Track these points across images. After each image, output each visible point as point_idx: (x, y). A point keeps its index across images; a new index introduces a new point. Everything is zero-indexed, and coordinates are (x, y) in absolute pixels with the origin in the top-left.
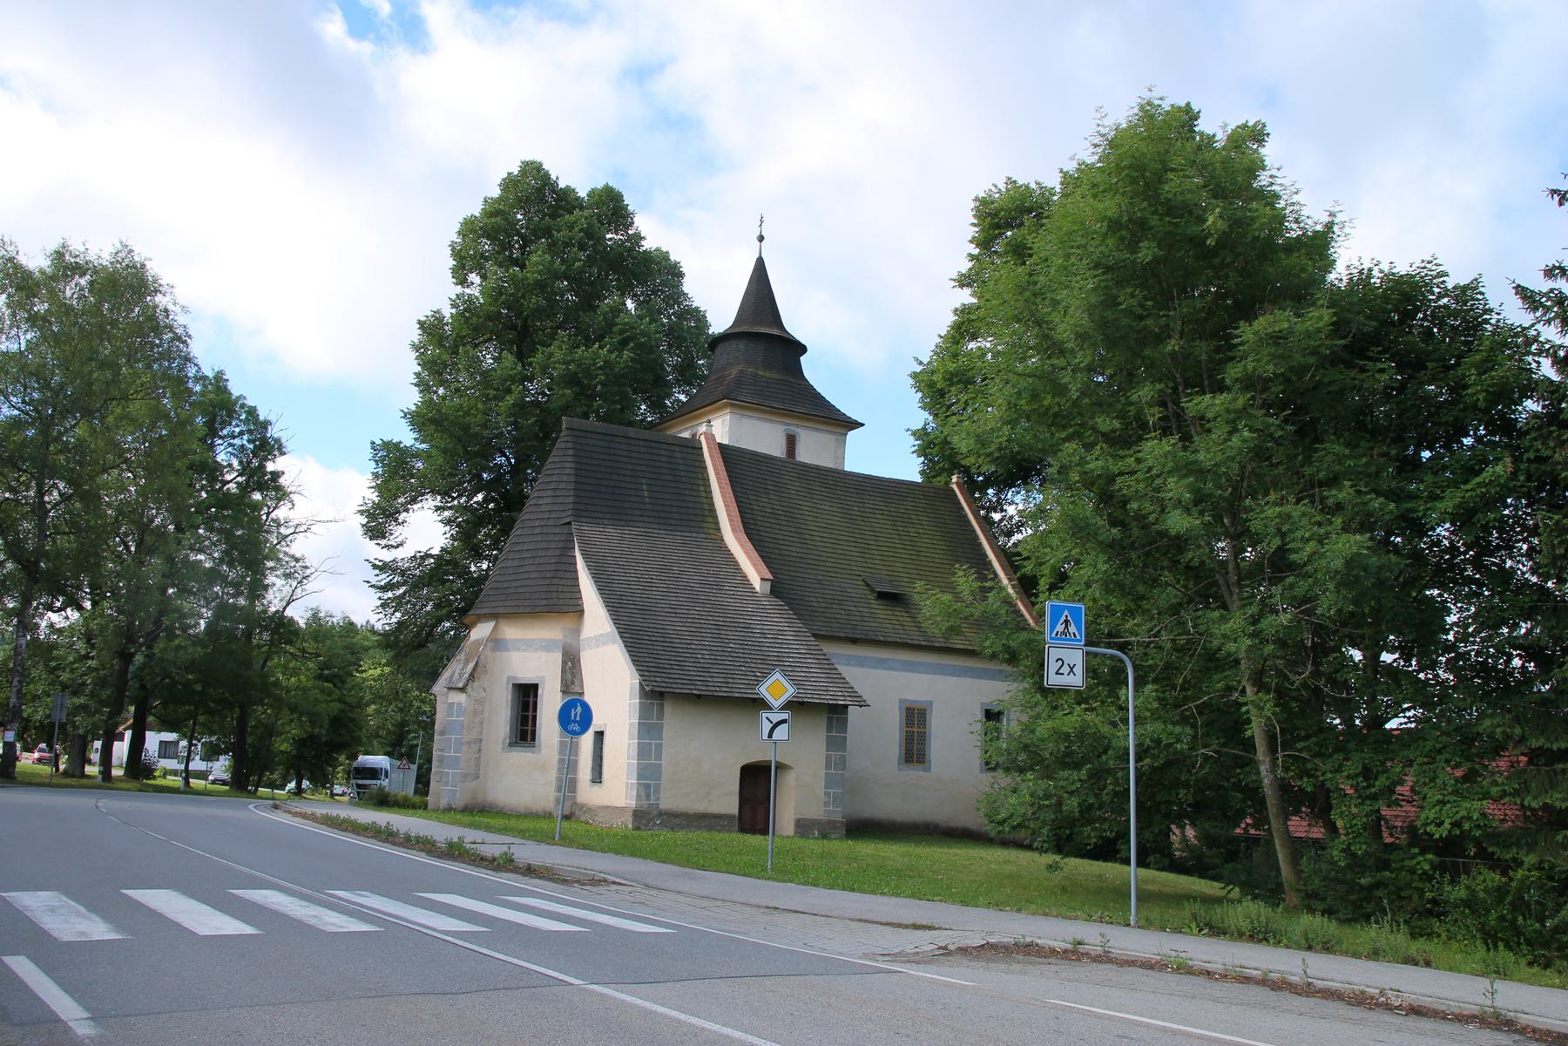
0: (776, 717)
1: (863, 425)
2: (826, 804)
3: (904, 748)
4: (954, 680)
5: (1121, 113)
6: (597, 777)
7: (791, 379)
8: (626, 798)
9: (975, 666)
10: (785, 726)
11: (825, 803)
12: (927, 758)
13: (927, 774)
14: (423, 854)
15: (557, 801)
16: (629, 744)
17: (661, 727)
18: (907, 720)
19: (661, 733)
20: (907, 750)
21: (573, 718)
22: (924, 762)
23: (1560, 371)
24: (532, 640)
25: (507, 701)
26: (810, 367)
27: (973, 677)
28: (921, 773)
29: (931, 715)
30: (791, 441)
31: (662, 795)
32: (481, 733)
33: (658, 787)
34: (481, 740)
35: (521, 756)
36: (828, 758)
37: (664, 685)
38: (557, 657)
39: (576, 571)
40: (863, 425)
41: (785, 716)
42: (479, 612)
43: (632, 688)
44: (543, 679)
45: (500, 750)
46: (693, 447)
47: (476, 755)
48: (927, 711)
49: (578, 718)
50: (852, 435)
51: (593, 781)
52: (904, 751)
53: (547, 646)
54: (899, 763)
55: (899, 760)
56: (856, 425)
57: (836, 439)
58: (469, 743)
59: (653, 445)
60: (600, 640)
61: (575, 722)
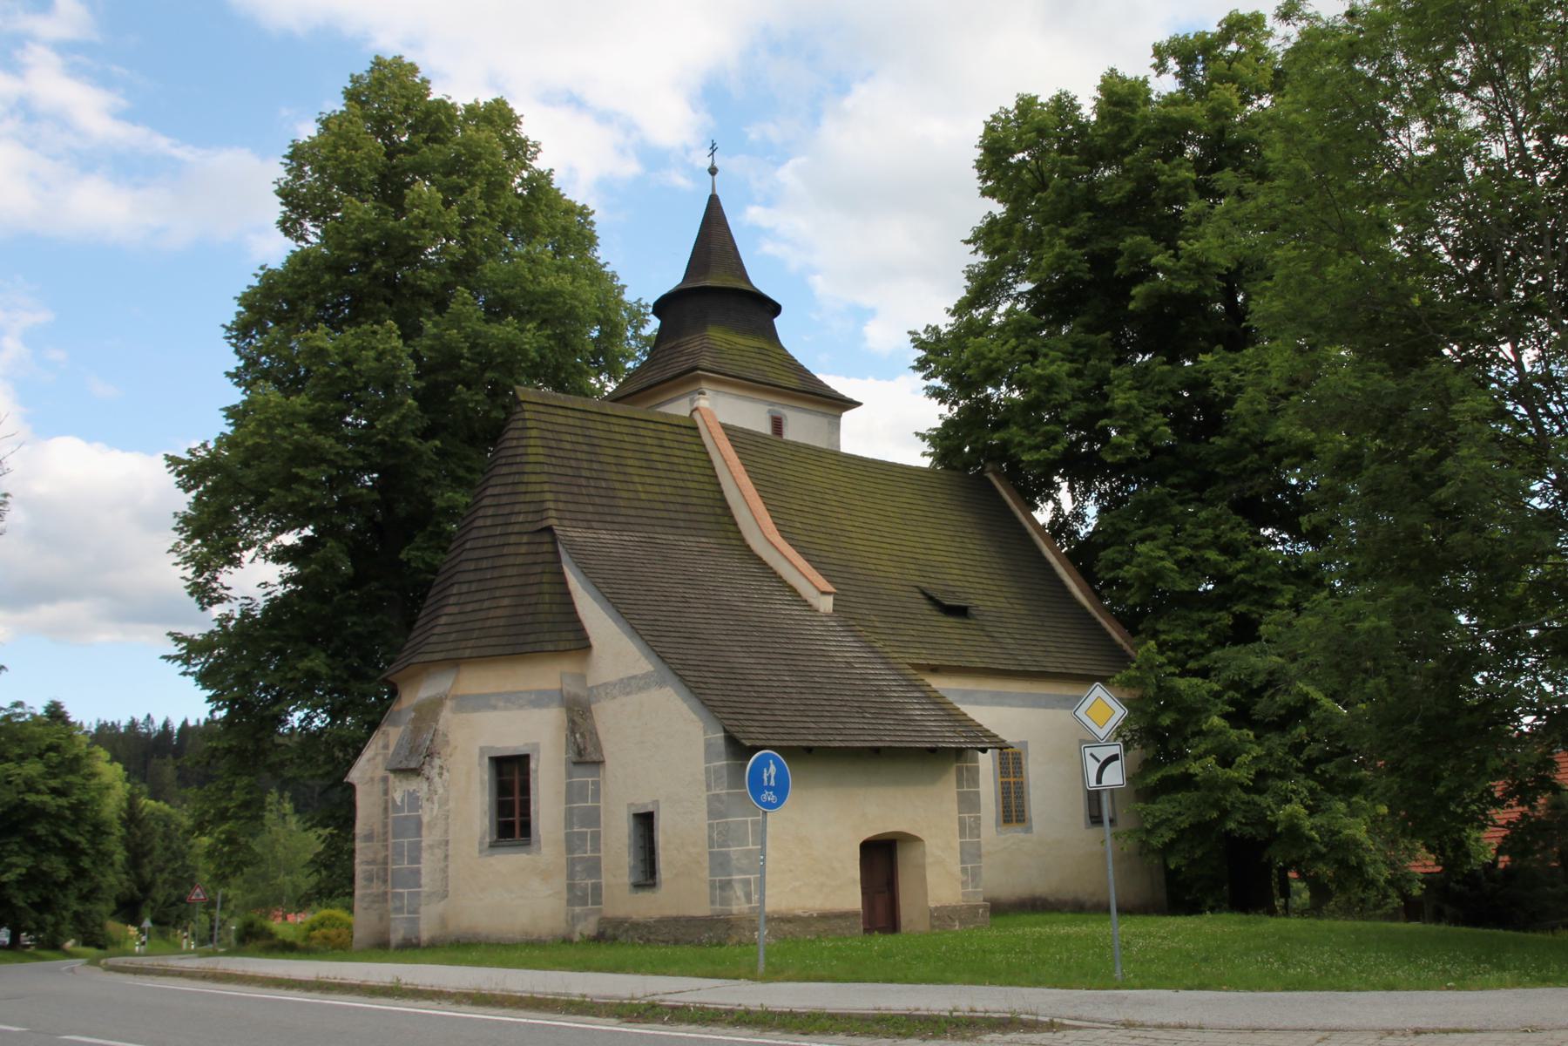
0: (1104, 753)
1: (859, 404)
2: (964, 884)
4: (1050, 712)
5: (1225, 14)
8: (713, 902)
9: (1058, 692)
10: (1116, 765)
14: (613, 1021)
18: (1002, 768)
20: (1004, 807)
21: (766, 783)
23: (1101, 427)
25: (482, 782)
28: (1022, 835)
30: (777, 424)
32: (446, 831)
35: (510, 861)
36: (962, 823)
40: (859, 404)
41: (1115, 750)
42: (427, 658)
44: (536, 746)
45: (476, 854)
46: (691, 428)
47: (442, 865)
49: (773, 783)
50: (847, 417)
51: (638, 886)
52: (1001, 809)
53: (539, 700)
54: (997, 826)
55: (997, 821)
56: (851, 404)
57: (829, 423)
58: (431, 847)
60: (628, 685)
61: (769, 788)
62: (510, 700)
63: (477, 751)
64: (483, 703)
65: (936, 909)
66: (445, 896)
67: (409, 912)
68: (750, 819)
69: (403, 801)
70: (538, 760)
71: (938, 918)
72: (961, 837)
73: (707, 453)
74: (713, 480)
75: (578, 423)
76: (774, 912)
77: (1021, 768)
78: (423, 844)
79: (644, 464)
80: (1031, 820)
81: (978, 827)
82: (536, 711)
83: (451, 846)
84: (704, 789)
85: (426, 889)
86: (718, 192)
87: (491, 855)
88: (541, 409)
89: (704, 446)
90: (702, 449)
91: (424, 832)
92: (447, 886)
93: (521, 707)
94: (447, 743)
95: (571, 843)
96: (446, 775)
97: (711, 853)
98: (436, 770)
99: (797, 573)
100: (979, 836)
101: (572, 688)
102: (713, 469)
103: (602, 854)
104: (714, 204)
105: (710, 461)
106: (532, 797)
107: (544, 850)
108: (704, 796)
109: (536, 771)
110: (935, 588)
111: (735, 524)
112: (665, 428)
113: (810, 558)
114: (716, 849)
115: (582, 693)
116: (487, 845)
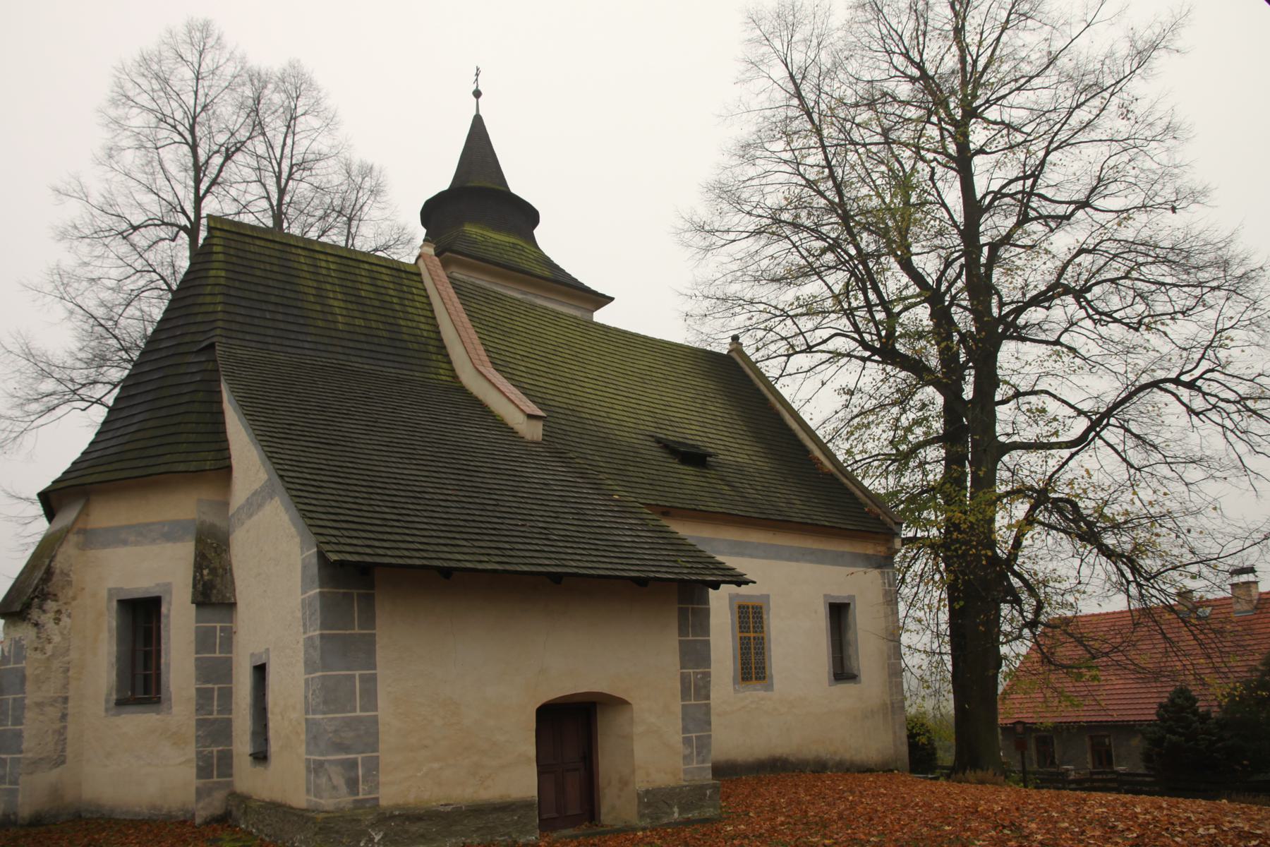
1: (612, 299)
2: (686, 758)
3: (739, 661)
6: (261, 757)
7: (525, 245)
8: (308, 791)
11: (685, 757)
12: (767, 673)
13: (769, 693)
15: (200, 793)
16: (307, 681)
17: (370, 643)
19: (371, 652)
22: (764, 678)
24: (148, 525)
26: (546, 238)
27: (811, 562)
28: (762, 693)
29: (768, 613)
31: (382, 778)
32: (65, 686)
33: (373, 766)
34: (66, 700)
35: (138, 721)
36: (684, 680)
37: (368, 551)
38: (186, 551)
39: (222, 413)
40: (612, 299)
43: (305, 567)
45: (103, 714)
47: (58, 726)
48: (764, 610)
52: (739, 666)
53: (171, 533)
55: (120, 590)
58: (40, 705)
59: (351, 263)
62: (142, 533)
63: (105, 594)
64: (116, 537)
65: (647, 792)
66: (60, 761)
67: (11, 783)
68: (357, 673)
69: (9, 652)
70: (170, 603)
71: (648, 805)
72: (683, 699)
73: (428, 297)
74: (430, 321)
75: (278, 254)
76: (397, 807)
77: (761, 622)
78: (27, 701)
79: (353, 299)
80: (771, 677)
81: (707, 686)
82: (169, 545)
83: (70, 704)
84: (302, 630)
85: (30, 755)
86: (481, 113)
87: (118, 714)
88: (235, 237)
89: (425, 290)
90: (423, 293)
91: (29, 686)
92: (63, 750)
93: (153, 541)
94: (70, 583)
95: (203, 697)
96: (65, 620)
97: (307, 720)
98: (51, 615)
99: (505, 400)
100: (708, 697)
101: (211, 518)
102: (432, 311)
103: (233, 716)
104: (478, 129)
105: (430, 304)
106: (163, 647)
107: (175, 709)
108: (302, 638)
109: (168, 616)
110: (671, 435)
111: (450, 362)
112: (384, 270)
113: (536, 399)
114: (310, 716)
115: (218, 522)
116: (112, 703)
